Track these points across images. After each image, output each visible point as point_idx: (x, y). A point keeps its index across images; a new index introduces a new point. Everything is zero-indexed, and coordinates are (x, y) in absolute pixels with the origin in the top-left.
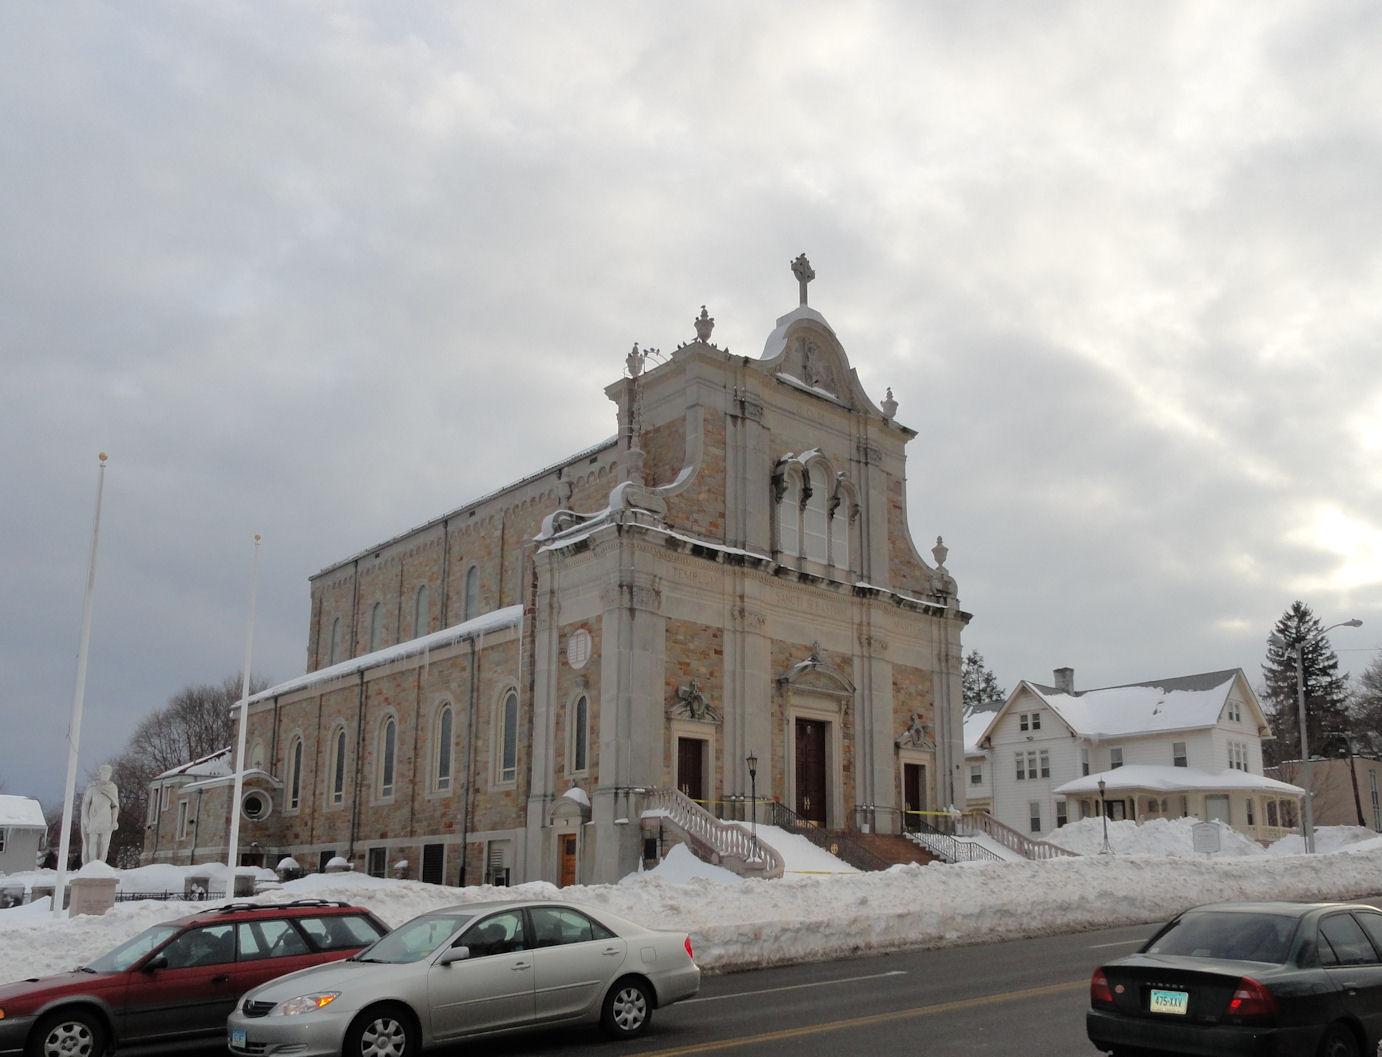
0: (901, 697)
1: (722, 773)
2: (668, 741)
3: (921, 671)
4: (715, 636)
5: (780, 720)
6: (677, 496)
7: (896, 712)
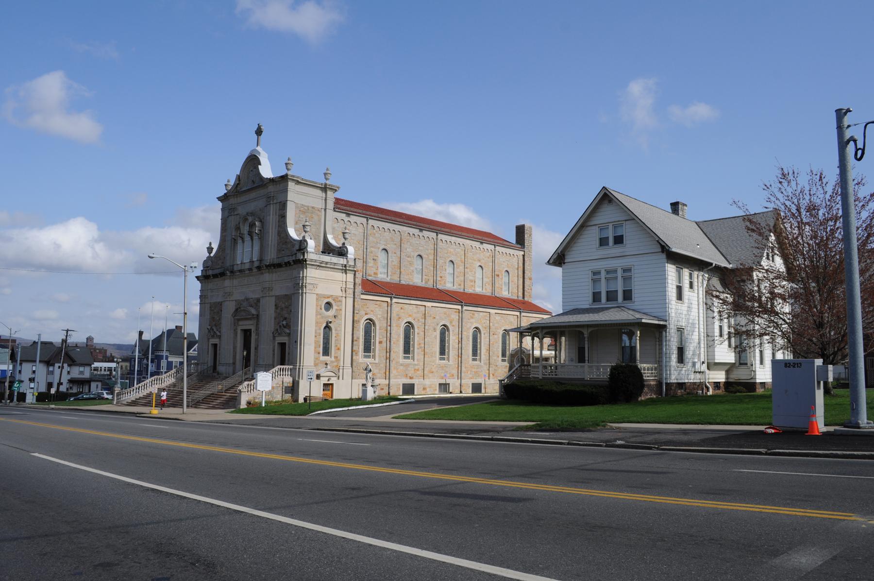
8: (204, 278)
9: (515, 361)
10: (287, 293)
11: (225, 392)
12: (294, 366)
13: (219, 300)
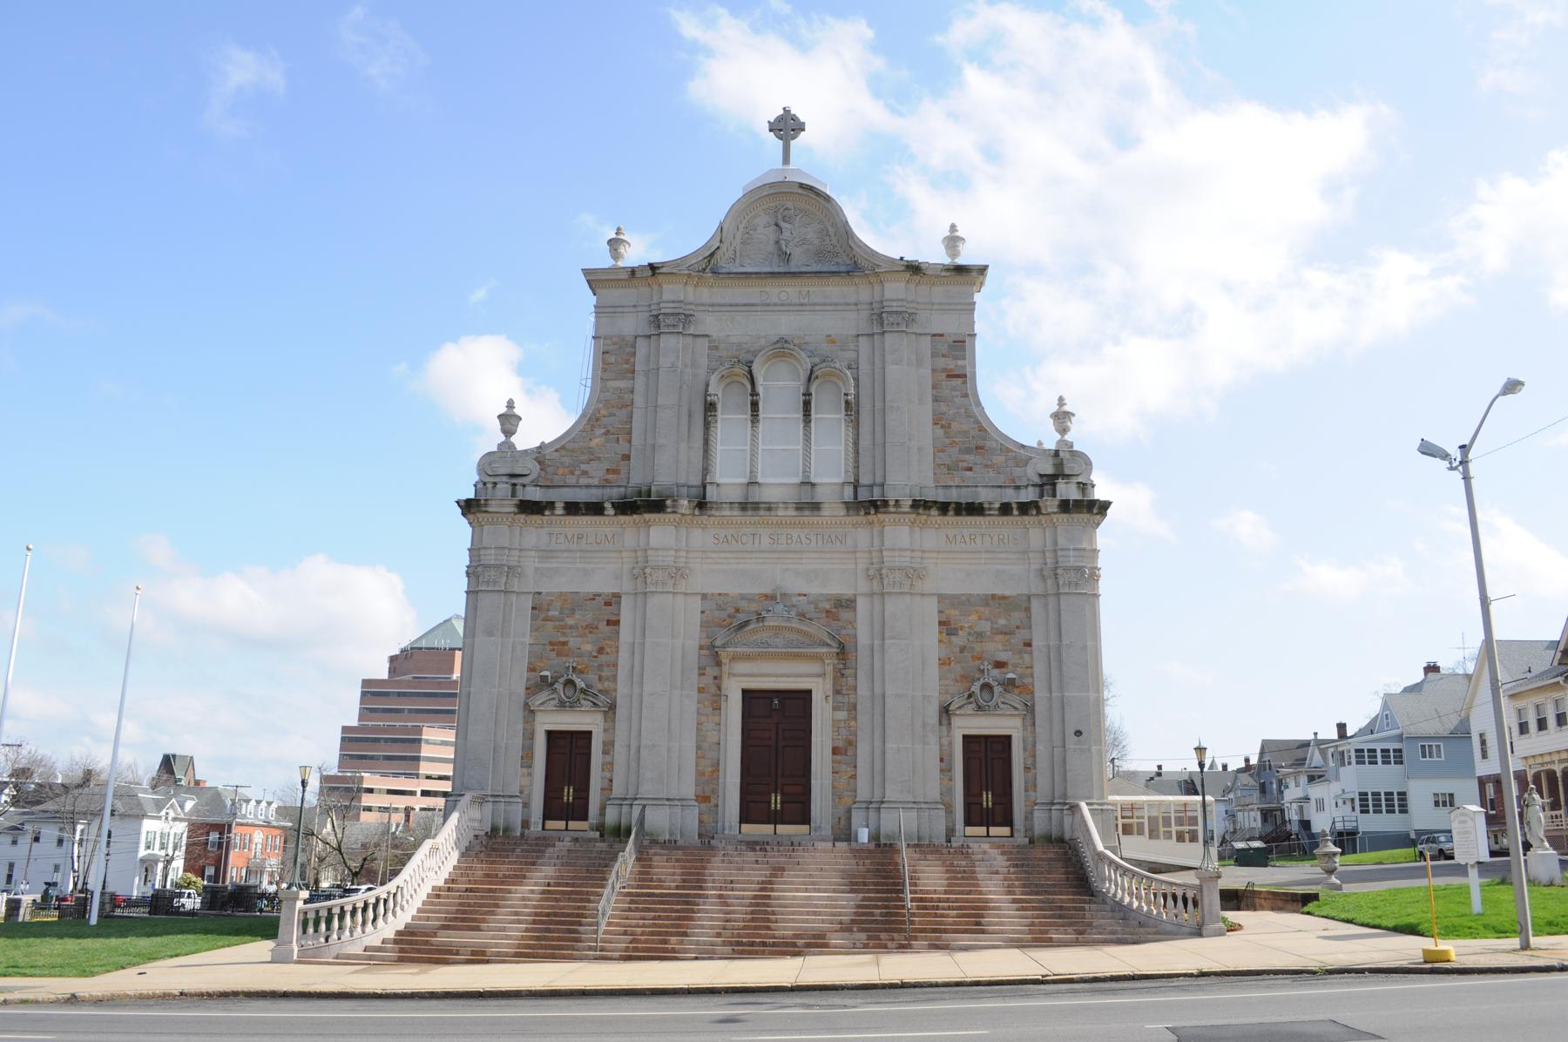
2: (529, 736)
3: (1004, 598)
4: (608, 604)
6: (557, 450)
7: (944, 662)
10: (999, 592)
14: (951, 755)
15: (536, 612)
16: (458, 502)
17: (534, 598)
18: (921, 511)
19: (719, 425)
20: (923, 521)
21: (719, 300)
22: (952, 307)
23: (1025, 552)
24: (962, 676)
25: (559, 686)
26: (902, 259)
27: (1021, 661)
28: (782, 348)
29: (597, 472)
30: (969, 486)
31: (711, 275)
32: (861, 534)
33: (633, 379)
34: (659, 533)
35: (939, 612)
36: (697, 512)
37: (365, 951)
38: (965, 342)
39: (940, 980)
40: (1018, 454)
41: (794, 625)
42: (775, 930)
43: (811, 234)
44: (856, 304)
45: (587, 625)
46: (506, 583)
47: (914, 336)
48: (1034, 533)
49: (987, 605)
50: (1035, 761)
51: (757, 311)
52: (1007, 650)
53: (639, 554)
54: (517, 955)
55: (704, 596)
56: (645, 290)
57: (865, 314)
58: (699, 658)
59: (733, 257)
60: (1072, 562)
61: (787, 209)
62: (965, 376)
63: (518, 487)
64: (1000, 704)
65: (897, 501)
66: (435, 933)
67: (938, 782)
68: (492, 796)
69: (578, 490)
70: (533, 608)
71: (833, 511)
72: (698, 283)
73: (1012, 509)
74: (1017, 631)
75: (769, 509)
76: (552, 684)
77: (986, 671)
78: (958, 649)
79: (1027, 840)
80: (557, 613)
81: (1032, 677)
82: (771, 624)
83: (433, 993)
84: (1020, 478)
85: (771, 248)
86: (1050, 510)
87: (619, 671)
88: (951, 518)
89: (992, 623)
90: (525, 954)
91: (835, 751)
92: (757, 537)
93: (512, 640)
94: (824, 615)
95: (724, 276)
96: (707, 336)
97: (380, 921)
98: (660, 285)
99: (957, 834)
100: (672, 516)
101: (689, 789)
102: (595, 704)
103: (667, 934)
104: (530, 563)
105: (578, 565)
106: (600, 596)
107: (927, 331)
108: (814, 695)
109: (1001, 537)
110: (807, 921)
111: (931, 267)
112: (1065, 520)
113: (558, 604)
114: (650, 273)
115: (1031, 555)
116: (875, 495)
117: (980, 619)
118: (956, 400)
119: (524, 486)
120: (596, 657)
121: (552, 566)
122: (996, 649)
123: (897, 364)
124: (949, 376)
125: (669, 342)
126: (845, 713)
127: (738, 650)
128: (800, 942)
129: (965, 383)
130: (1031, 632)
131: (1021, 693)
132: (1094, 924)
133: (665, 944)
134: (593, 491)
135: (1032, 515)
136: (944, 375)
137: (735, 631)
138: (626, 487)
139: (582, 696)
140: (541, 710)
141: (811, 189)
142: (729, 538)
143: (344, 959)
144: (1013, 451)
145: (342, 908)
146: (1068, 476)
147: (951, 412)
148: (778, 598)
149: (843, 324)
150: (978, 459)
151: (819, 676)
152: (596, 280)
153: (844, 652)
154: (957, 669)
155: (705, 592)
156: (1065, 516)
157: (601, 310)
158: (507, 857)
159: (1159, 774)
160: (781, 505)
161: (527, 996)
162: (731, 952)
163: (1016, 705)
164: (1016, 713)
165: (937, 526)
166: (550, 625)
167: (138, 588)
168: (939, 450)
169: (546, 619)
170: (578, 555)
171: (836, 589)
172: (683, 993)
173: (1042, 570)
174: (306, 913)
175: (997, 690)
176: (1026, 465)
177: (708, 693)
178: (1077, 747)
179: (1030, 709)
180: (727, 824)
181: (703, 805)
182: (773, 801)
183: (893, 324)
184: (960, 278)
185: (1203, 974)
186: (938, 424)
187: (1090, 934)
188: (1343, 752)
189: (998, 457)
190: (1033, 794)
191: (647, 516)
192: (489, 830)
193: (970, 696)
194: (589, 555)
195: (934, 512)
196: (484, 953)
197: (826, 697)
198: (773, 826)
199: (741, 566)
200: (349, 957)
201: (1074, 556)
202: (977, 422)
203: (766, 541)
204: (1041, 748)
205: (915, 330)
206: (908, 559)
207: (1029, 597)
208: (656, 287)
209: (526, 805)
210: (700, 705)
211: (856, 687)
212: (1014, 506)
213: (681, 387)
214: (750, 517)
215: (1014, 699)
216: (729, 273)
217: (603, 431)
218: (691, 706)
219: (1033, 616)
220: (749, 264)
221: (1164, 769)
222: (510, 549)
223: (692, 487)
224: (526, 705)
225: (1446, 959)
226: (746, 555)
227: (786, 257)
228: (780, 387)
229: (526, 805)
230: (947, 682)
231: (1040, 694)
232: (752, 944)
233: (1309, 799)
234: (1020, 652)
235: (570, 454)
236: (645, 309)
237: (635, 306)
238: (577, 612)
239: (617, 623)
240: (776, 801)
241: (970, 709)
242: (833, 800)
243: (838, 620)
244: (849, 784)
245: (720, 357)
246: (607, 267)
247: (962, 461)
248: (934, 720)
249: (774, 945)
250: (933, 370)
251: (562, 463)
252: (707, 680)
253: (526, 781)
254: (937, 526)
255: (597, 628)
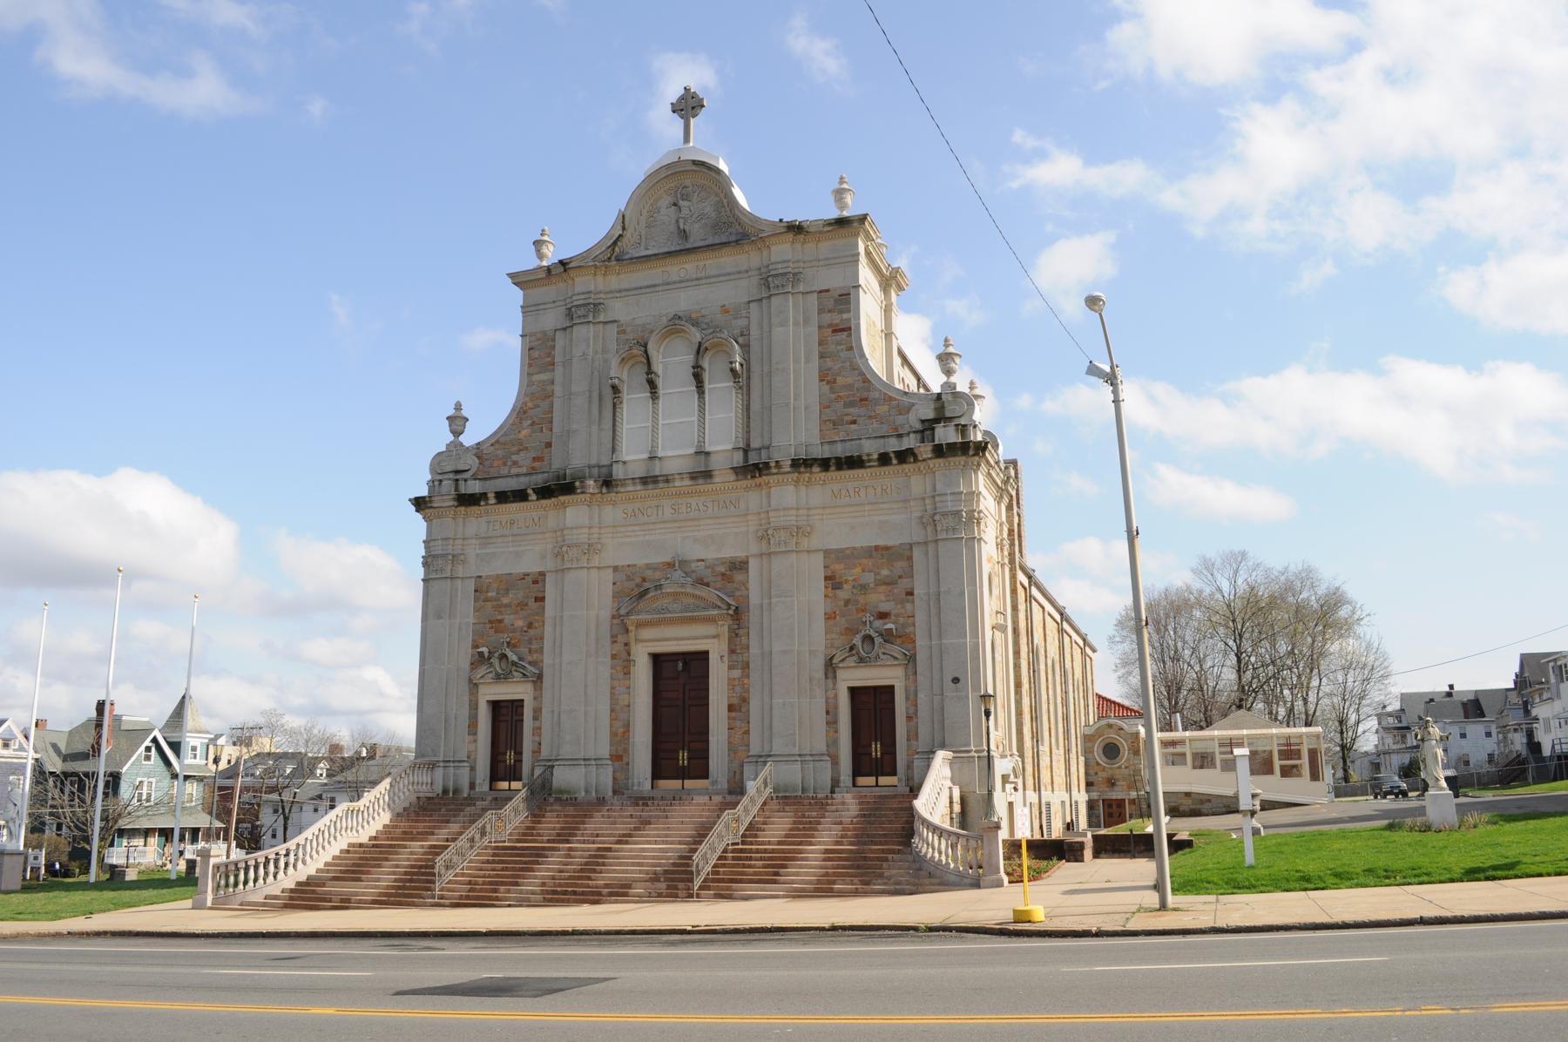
0: (843, 594)
1: (540, 735)
2: (474, 706)
3: (887, 548)
4: (535, 582)
5: (623, 663)
6: (492, 445)
7: (829, 617)
8: (456, 503)
9: (1095, 750)
10: (881, 542)
11: (743, 843)
12: (954, 752)
13: (530, 565)
14: (836, 707)
15: (478, 594)
16: (410, 500)
17: (476, 581)
18: (802, 469)
19: (625, 405)
20: (807, 479)
21: (625, 285)
22: (838, 261)
23: (906, 501)
24: (847, 629)
25: (495, 661)
26: (781, 220)
27: (903, 611)
28: (675, 326)
29: (524, 460)
30: (852, 440)
31: (615, 263)
32: (751, 497)
33: (553, 370)
34: (574, 514)
35: (825, 567)
36: (604, 490)
37: (265, 899)
38: (849, 294)
39: (603, 929)
40: (900, 402)
41: (688, 590)
42: (594, 880)
43: (708, 208)
44: (747, 272)
45: (518, 604)
46: (451, 570)
47: (801, 295)
48: (915, 481)
49: (871, 556)
50: (916, 711)
51: (659, 291)
52: (888, 601)
53: (762, 515)
54: (374, 902)
55: (616, 569)
56: (562, 285)
57: (755, 280)
58: (611, 626)
59: (638, 241)
60: (950, 507)
61: (685, 187)
62: (850, 329)
63: (460, 482)
64: (880, 655)
65: (777, 462)
66: (324, 883)
67: (825, 734)
68: (444, 761)
69: (509, 479)
70: (476, 591)
71: (723, 478)
72: (805, 239)
73: (891, 459)
74: (900, 581)
75: (667, 481)
76: (489, 658)
77: (868, 623)
78: (842, 603)
79: (908, 788)
80: (494, 594)
81: (914, 626)
82: (669, 591)
83: (231, 933)
84: (902, 426)
85: (673, 228)
86: (924, 456)
87: (545, 642)
88: (833, 474)
89: (875, 575)
90: (823, 889)
91: (731, 708)
92: (660, 508)
93: (458, 621)
94: (720, 578)
95: (627, 262)
96: (615, 321)
97: (281, 875)
98: (573, 279)
99: (842, 785)
100: (582, 496)
101: (604, 750)
102: (524, 675)
103: (497, 883)
104: (472, 551)
105: (511, 549)
106: (528, 575)
107: (813, 289)
108: (711, 656)
109: (885, 487)
110: (626, 872)
111: (812, 223)
112: (942, 465)
113: (495, 586)
114: (562, 269)
115: (912, 503)
116: (763, 457)
117: (863, 571)
118: (842, 354)
119: (466, 480)
120: (525, 631)
121: (489, 551)
122: (879, 599)
123: (782, 326)
124: (835, 331)
125: (580, 332)
126: (740, 671)
127: (640, 617)
128: (605, 891)
129: (850, 335)
130: (913, 581)
131: (903, 642)
132: (885, 875)
133: (496, 892)
134: (522, 479)
135: (910, 463)
136: (830, 330)
137: (638, 600)
138: (548, 472)
139: (514, 668)
140: (483, 683)
141: (702, 164)
142: (636, 511)
143: (249, 907)
144: (895, 399)
145: (256, 860)
146: (951, 419)
147: (836, 367)
148: (677, 565)
149: (735, 292)
150: (862, 411)
151: (714, 637)
152: (520, 280)
153: (738, 615)
154: (842, 622)
155: (616, 565)
156: (941, 460)
157: (528, 310)
158: (431, 816)
159: (1449, 695)
160: (677, 477)
161: (295, 936)
162: (542, 899)
163: (896, 655)
164: (896, 663)
165: (821, 482)
166: (489, 604)
167: (196, 597)
168: (824, 406)
169: (486, 600)
170: (510, 539)
171: (731, 552)
172: (405, 936)
173: (922, 517)
174: (227, 866)
175: (878, 640)
176: (908, 412)
177: (620, 659)
178: (955, 694)
179: (911, 660)
180: (636, 781)
181: (616, 763)
182: (681, 758)
183: (778, 287)
184: (843, 231)
185: (834, 928)
186: (823, 380)
187: (875, 885)
188: (1561, 666)
189: (881, 407)
190: (915, 743)
191: (562, 498)
192: (440, 792)
193: (852, 648)
194: (519, 538)
195: (816, 469)
196: (349, 901)
197: (722, 657)
198: (681, 781)
199: (647, 538)
200: (249, 904)
201: (951, 501)
202: (862, 374)
203: (668, 512)
204: (922, 696)
205: (801, 290)
206: (794, 518)
207: (911, 546)
208: (570, 282)
209: (473, 769)
210: (614, 671)
211: (748, 646)
212: (892, 455)
213: (593, 373)
214: (651, 491)
215: (895, 649)
216: (632, 259)
217: (529, 422)
218: (605, 672)
219: (914, 564)
220: (654, 246)
221: (1456, 688)
222: (454, 539)
223: (603, 466)
224: (470, 680)
225: (1027, 920)
226: (651, 527)
227: (684, 234)
228: (672, 362)
229: (473, 769)
230: (833, 636)
231: (921, 642)
232: (565, 893)
233: (1538, 719)
234: (902, 602)
235: (502, 446)
236: (757, 273)
237: (554, 302)
238: (510, 592)
239: (542, 599)
240: (683, 757)
241: (851, 661)
242: (729, 755)
243: (733, 582)
244: (743, 739)
245: (627, 340)
246: (531, 268)
247: (847, 415)
248: (821, 674)
249: (583, 893)
250: (819, 327)
251: (496, 456)
252: (619, 647)
253: (472, 747)
254: (821, 482)
255: (527, 605)
